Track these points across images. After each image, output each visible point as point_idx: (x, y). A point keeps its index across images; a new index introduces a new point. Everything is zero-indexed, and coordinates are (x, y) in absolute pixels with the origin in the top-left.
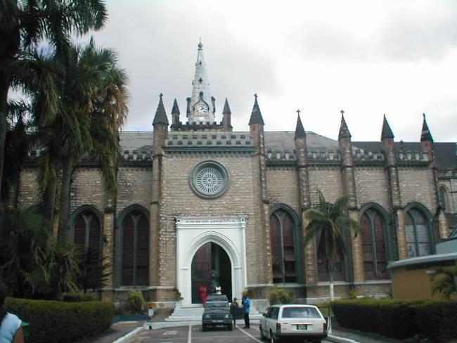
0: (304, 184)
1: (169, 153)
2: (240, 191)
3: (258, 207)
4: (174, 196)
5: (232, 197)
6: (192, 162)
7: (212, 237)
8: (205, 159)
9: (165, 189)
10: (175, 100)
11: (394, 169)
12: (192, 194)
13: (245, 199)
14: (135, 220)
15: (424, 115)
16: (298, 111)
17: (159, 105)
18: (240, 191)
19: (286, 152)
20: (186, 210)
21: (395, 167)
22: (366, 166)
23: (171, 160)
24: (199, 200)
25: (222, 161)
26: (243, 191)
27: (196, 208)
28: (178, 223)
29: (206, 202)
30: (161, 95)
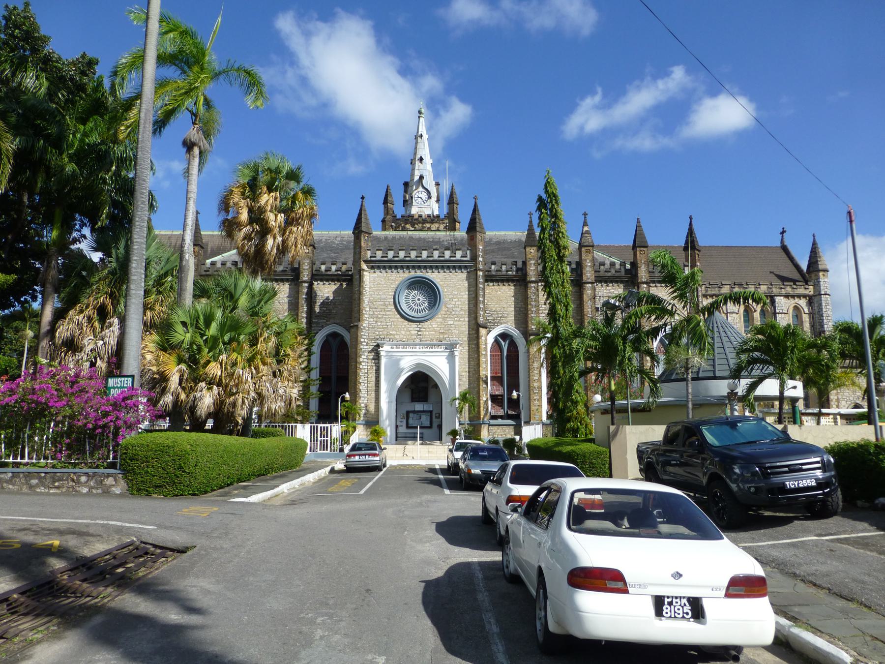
0: (533, 304)
1: (372, 268)
2: (453, 313)
3: (474, 332)
4: (377, 317)
5: (444, 318)
6: (399, 277)
7: (418, 365)
8: (413, 273)
9: (367, 309)
10: (638, 221)
11: (645, 286)
12: (399, 316)
13: (460, 323)
14: (505, 346)
15: (814, 236)
16: (363, 198)
17: (813, 248)
18: (453, 313)
19: (503, 264)
20: (391, 334)
21: (646, 283)
22: (611, 282)
23: (373, 275)
24: (406, 323)
25: (435, 276)
26: (457, 313)
27: (403, 333)
28: (381, 349)
29: (414, 325)
30: (585, 214)
